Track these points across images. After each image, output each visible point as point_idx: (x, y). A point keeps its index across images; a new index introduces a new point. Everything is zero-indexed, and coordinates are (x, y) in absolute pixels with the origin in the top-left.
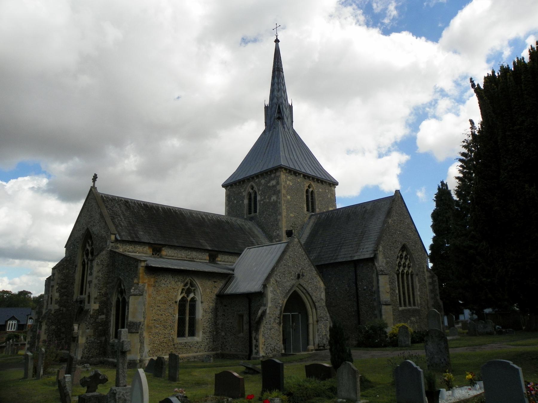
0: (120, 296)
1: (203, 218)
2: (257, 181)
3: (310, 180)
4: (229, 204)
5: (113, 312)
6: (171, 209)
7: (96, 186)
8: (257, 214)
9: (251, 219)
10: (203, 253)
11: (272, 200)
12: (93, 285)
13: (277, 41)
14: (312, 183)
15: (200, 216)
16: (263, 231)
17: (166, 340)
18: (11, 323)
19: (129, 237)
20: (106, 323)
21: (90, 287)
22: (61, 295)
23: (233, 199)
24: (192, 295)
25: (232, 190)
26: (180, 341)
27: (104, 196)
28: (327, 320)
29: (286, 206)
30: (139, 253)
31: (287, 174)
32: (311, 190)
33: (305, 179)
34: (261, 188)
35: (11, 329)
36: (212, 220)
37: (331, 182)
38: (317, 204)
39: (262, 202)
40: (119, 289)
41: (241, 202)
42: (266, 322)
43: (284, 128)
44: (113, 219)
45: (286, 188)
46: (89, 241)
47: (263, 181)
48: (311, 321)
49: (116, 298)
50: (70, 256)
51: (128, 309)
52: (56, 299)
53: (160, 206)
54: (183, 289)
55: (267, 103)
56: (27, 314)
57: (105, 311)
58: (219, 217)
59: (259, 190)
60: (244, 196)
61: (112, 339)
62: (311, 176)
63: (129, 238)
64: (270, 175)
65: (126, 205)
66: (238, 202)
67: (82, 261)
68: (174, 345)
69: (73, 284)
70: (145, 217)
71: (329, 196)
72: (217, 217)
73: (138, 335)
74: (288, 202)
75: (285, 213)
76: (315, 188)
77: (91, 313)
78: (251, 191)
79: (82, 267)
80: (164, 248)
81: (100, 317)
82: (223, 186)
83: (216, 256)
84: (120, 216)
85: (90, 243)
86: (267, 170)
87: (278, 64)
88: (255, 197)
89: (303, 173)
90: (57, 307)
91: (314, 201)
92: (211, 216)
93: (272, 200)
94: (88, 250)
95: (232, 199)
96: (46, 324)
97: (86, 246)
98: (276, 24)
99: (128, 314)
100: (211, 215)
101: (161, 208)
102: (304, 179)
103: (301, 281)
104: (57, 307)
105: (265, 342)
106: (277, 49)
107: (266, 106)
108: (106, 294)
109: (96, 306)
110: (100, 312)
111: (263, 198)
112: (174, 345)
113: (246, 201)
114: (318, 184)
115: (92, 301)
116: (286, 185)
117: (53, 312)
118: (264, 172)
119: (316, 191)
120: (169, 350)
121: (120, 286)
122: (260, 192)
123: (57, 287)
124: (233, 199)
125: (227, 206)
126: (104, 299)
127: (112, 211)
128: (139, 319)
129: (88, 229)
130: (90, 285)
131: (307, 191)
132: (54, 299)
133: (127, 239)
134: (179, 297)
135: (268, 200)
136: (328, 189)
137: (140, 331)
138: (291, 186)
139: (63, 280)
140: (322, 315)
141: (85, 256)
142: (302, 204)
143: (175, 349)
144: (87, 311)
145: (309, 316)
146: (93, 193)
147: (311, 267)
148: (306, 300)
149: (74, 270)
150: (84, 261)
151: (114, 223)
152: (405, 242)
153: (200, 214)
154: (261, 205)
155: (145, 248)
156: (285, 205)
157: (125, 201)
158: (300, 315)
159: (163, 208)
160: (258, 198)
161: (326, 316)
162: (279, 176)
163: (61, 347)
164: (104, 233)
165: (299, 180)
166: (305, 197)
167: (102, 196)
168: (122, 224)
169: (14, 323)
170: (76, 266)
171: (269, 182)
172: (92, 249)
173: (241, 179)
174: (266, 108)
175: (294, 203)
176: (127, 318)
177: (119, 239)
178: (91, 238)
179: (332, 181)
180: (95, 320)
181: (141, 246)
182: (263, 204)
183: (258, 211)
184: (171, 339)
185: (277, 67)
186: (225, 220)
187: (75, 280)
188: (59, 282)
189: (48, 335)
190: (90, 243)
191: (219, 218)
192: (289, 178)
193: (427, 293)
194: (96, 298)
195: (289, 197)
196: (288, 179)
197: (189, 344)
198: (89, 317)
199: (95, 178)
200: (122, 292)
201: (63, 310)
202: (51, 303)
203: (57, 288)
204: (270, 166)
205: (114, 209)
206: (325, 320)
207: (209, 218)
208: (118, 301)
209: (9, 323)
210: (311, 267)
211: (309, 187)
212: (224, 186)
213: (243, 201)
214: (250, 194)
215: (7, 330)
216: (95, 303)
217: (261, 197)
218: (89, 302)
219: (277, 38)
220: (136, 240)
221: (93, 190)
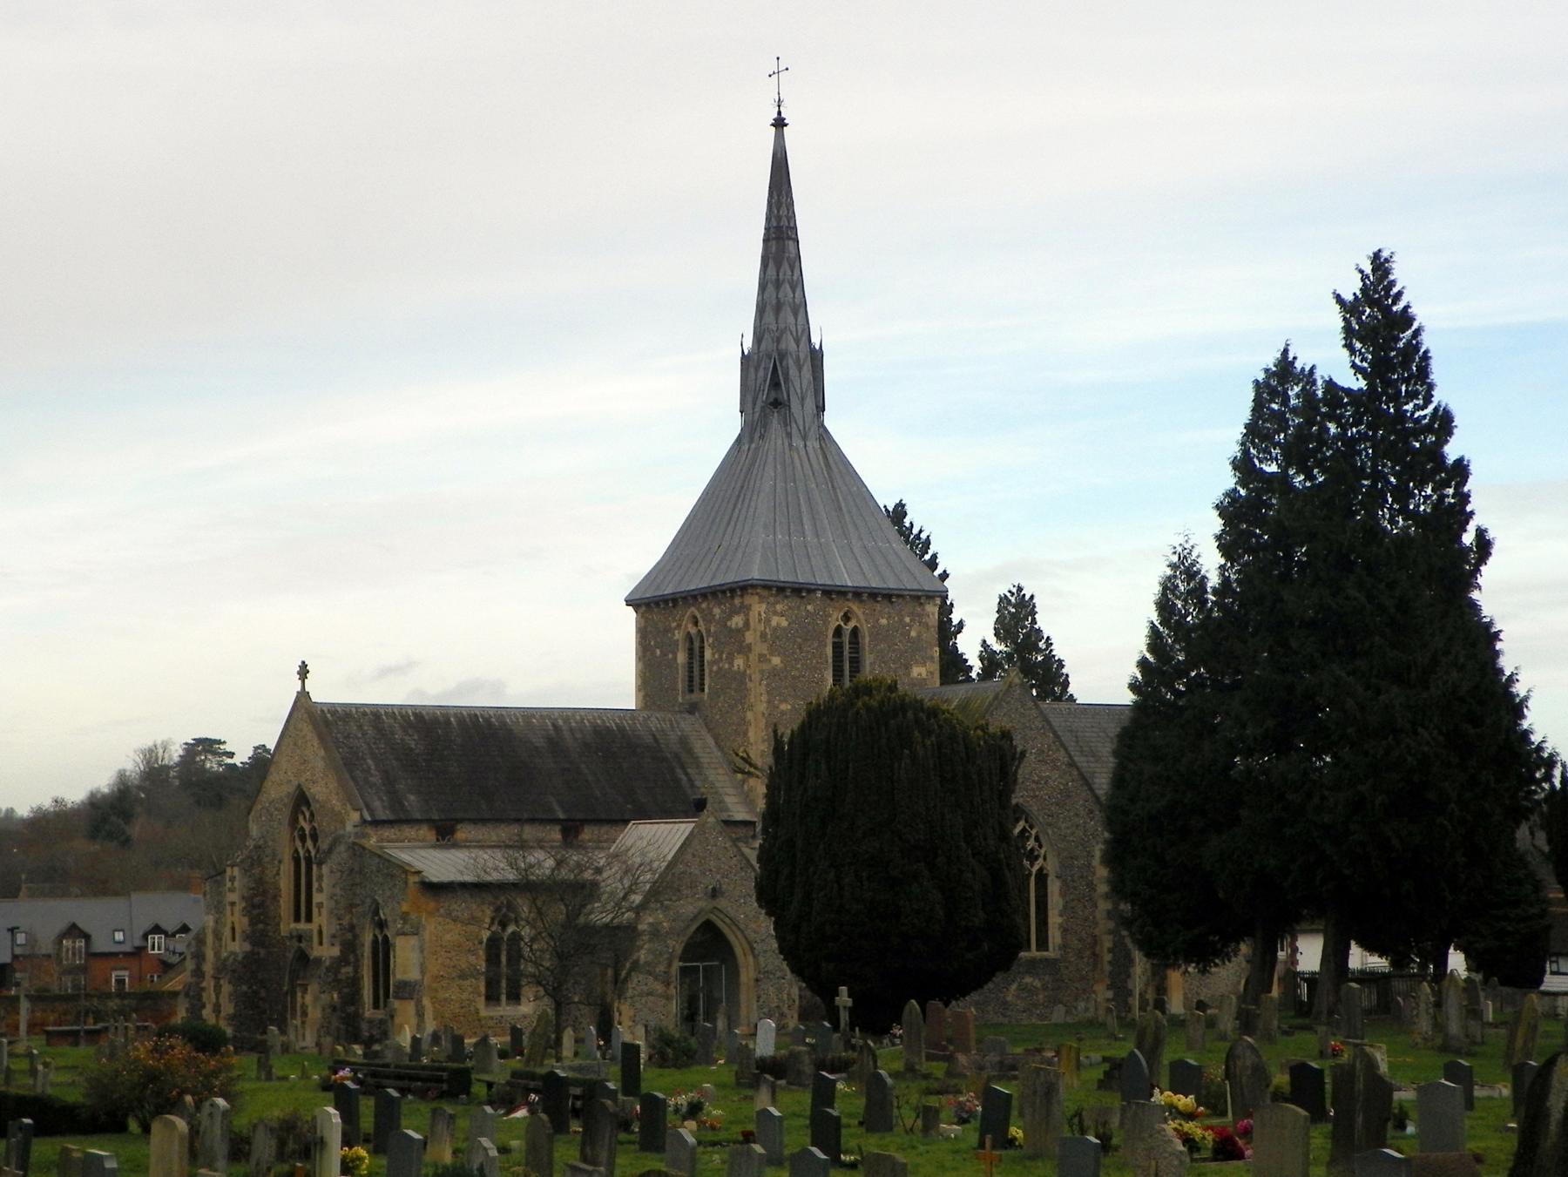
0: (377, 932)
1: (555, 726)
2: (704, 606)
3: (848, 600)
6: (478, 713)
7: (307, 690)
8: (706, 697)
9: (693, 709)
10: (548, 827)
11: (736, 668)
12: (324, 911)
13: (779, 123)
15: (549, 724)
16: (716, 743)
17: (463, 1011)
20: (355, 982)
22: (253, 923)
23: (652, 643)
24: (511, 929)
25: (650, 617)
26: (491, 1014)
28: (784, 978)
30: (409, 841)
31: (772, 599)
32: (852, 624)
33: (832, 599)
34: (712, 629)
37: (920, 593)
38: (868, 662)
39: (715, 668)
40: (376, 918)
42: (639, 982)
45: (769, 636)
47: (717, 611)
48: (743, 978)
49: (371, 935)
50: (263, 837)
51: (394, 957)
54: (493, 919)
55: (748, 344)
56: (10, 927)
58: (600, 718)
59: (708, 631)
60: (678, 640)
61: (369, 1010)
62: (851, 589)
64: (732, 597)
67: (292, 851)
69: (276, 898)
71: (913, 634)
72: (594, 717)
73: (412, 1003)
76: (862, 617)
80: (461, 825)
81: (344, 970)
83: (577, 832)
85: (307, 815)
86: (723, 585)
87: (778, 212)
89: (821, 588)
91: (860, 654)
92: (578, 718)
93: (736, 668)
94: (302, 829)
95: (650, 643)
98: (778, 58)
99: (395, 966)
100: (581, 716)
101: (455, 715)
102: (828, 601)
103: (722, 903)
105: (635, 1016)
106: (779, 155)
108: (352, 928)
110: (342, 960)
111: (716, 656)
113: (681, 658)
114: (878, 607)
116: (767, 630)
118: (718, 588)
119: (865, 629)
120: (470, 1029)
121: (376, 912)
124: (652, 643)
125: (640, 659)
128: (413, 975)
129: (299, 786)
130: (319, 911)
131: (838, 632)
132: (238, 930)
134: (485, 935)
135: (727, 666)
136: (911, 614)
137: (415, 996)
139: (253, 889)
140: (770, 968)
142: (818, 671)
143: (482, 1027)
145: (741, 970)
147: (746, 872)
148: (732, 938)
149: (276, 869)
150: (296, 851)
153: (550, 718)
154: (713, 674)
155: (420, 829)
158: (723, 966)
159: (459, 715)
160: (708, 654)
161: (782, 970)
162: (749, 608)
163: (261, 1031)
164: (338, 804)
166: (829, 650)
171: (730, 617)
172: (314, 829)
173: (667, 595)
174: (745, 359)
176: (394, 976)
178: (308, 804)
179: (924, 590)
180: (336, 975)
181: (412, 827)
182: (717, 673)
183: (706, 690)
184: (472, 1009)
185: (775, 224)
188: (246, 895)
189: (236, 1006)
190: (307, 815)
191: (599, 721)
192: (779, 607)
194: (334, 936)
195: (776, 660)
196: (775, 613)
197: (509, 1019)
198: (325, 970)
199: (303, 672)
204: (731, 578)
206: (778, 978)
208: (375, 941)
210: (746, 872)
212: (630, 603)
214: (689, 638)
217: (713, 654)
219: (779, 113)
220: (402, 816)
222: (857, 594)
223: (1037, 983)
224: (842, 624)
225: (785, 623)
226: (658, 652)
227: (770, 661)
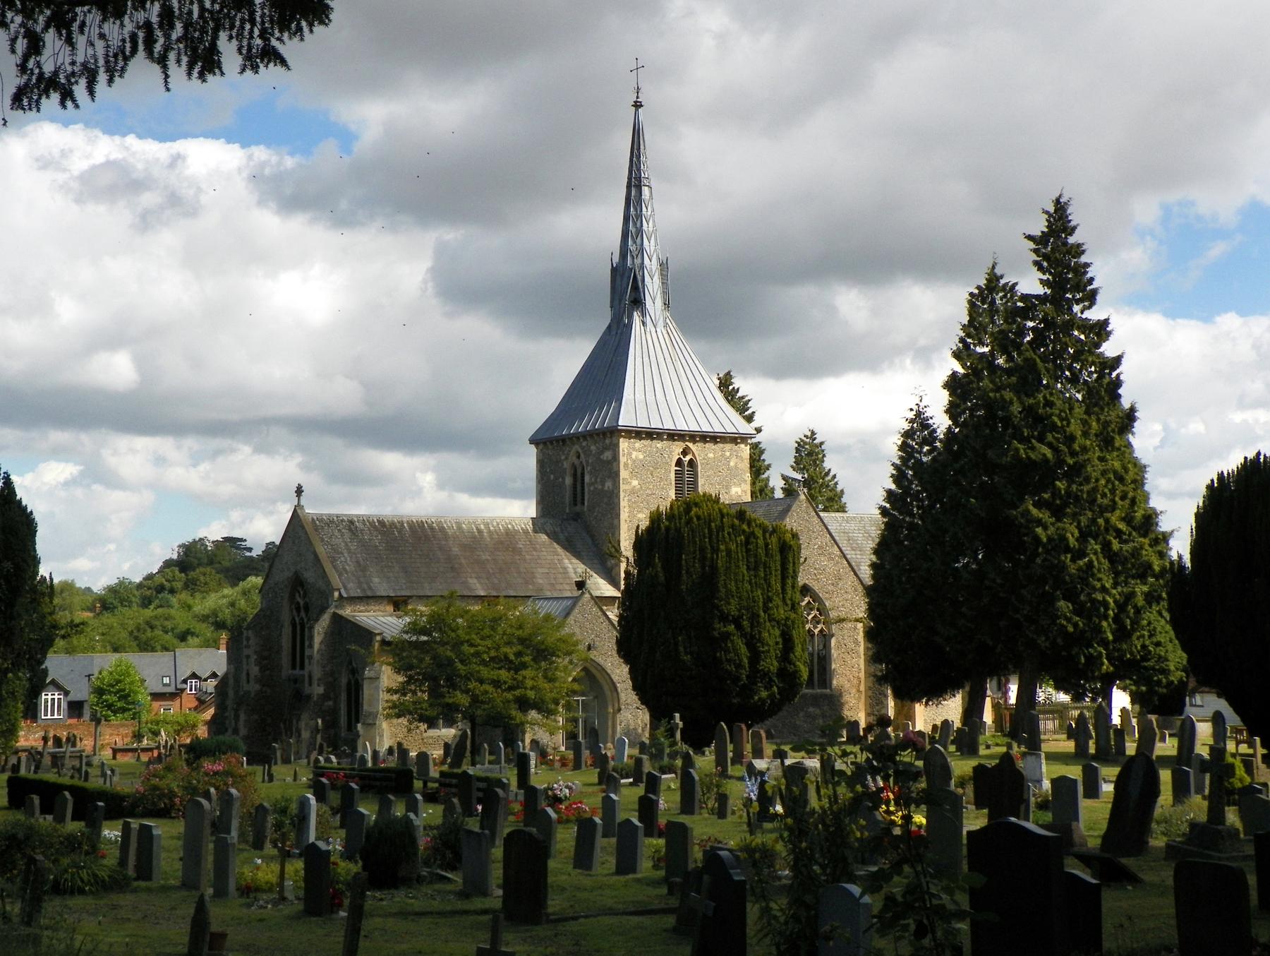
0: (351, 676)
1: (480, 531)
4: (542, 479)
5: (343, 697)
8: (585, 509)
14: (690, 445)
18: (50, 697)
19: (359, 591)
20: (334, 712)
21: (310, 664)
22: (263, 669)
27: (315, 518)
29: (629, 500)
34: (590, 461)
35: (53, 714)
36: (497, 533)
41: (560, 480)
43: (644, 323)
44: (333, 561)
46: (300, 589)
52: (256, 676)
53: (405, 520)
57: (332, 695)
58: (510, 523)
63: (359, 593)
65: (350, 530)
66: (556, 479)
68: (423, 739)
70: (381, 548)
71: (732, 464)
74: (633, 492)
75: (627, 514)
77: (315, 699)
78: (577, 462)
79: (290, 629)
81: (326, 704)
82: (533, 441)
84: (342, 554)
85: (302, 593)
88: (583, 475)
90: (257, 687)
92: (495, 524)
94: (298, 603)
96: (245, 713)
97: (294, 596)
104: (257, 687)
107: (615, 265)
109: (321, 690)
110: (325, 697)
112: (423, 739)
113: (568, 481)
114: (707, 445)
115: (315, 682)
117: (252, 695)
121: (350, 663)
122: (589, 468)
123: (255, 657)
126: (331, 679)
127: (332, 545)
132: (252, 676)
133: (356, 595)
138: (641, 461)
141: (294, 611)
144: (309, 697)
146: (298, 516)
150: (294, 619)
151: (335, 567)
152: (807, 582)
156: (626, 498)
157: (349, 521)
160: (587, 479)
165: (658, 445)
167: (313, 519)
168: (347, 567)
169: (56, 697)
170: (282, 626)
175: (648, 491)
177: (345, 595)
183: (586, 504)
186: (522, 528)
187: (281, 647)
190: (302, 593)
191: (509, 526)
193: (859, 665)
194: (319, 680)
195: (635, 483)
196: (634, 449)
199: (299, 491)
200: (354, 672)
201: (266, 692)
202: (248, 682)
203: (256, 659)
205: (334, 541)
207: (492, 528)
208: (349, 683)
209: (44, 697)
211: (685, 453)
213: (564, 479)
214: (574, 467)
215: (43, 717)
216: (319, 685)
218: (310, 684)
220: (369, 594)
221: (299, 511)
222: (694, 437)
223: (818, 711)
224: (682, 457)
225: (641, 457)
226: (552, 477)
227: (630, 483)
